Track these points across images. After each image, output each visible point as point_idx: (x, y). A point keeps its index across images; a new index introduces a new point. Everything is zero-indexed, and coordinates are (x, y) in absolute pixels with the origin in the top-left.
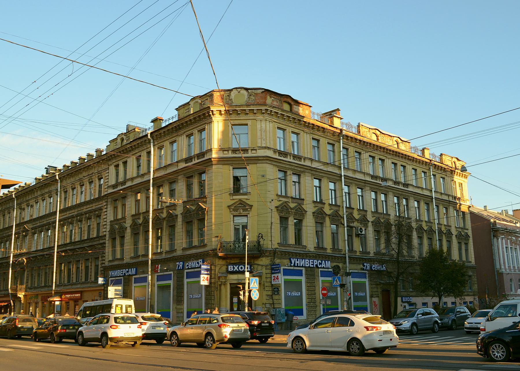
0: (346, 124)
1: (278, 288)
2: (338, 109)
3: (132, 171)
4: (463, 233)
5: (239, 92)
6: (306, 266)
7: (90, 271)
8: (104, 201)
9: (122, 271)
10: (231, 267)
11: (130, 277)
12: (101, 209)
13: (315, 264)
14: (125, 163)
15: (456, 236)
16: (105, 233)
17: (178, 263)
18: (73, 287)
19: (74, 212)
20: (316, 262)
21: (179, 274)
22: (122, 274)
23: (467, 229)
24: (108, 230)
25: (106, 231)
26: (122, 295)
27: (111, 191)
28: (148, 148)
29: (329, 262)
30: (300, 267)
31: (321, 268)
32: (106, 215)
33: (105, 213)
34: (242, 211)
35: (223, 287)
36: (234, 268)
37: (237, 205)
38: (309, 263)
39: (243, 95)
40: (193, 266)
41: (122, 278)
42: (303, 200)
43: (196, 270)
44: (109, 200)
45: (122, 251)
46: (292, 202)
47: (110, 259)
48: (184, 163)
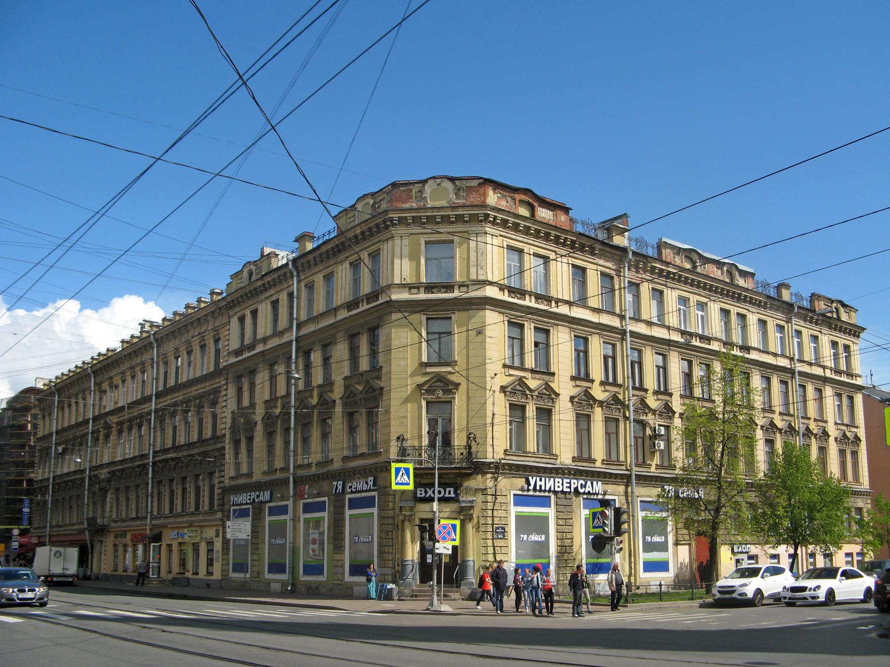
0: (636, 241)
1: (503, 528)
2: (625, 214)
3: (264, 327)
4: (848, 434)
5: (439, 185)
6: (557, 489)
7: (202, 492)
8: (222, 378)
9: (250, 496)
10: (421, 491)
11: (263, 505)
12: (217, 391)
13: (573, 486)
14: (254, 313)
15: (836, 439)
16: (223, 431)
17: (335, 483)
18: (178, 520)
19: (178, 397)
20: (574, 483)
21: (338, 499)
22: (250, 499)
23: (857, 427)
24: (228, 426)
25: (225, 429)
26: (250, 535)
27: (233, 360)
28: (290, 286)
29: (600, 483)
30: (545, 491)
31: (584, 493)
32: (226, 401)
33: (225, 398)
34: (440, 393)
35: (407, 524)
36: (426, 492)
37: (433, 383)
38: (562, 484)
39: (447, 190)
40: (359, 487)
41: (250, 506)
42: (553, 374)
43: (364, 495)
44: (231, 376)
45: (250, 464)
46: (532, 378)
47: (232, 474)
48: (346, 310)
